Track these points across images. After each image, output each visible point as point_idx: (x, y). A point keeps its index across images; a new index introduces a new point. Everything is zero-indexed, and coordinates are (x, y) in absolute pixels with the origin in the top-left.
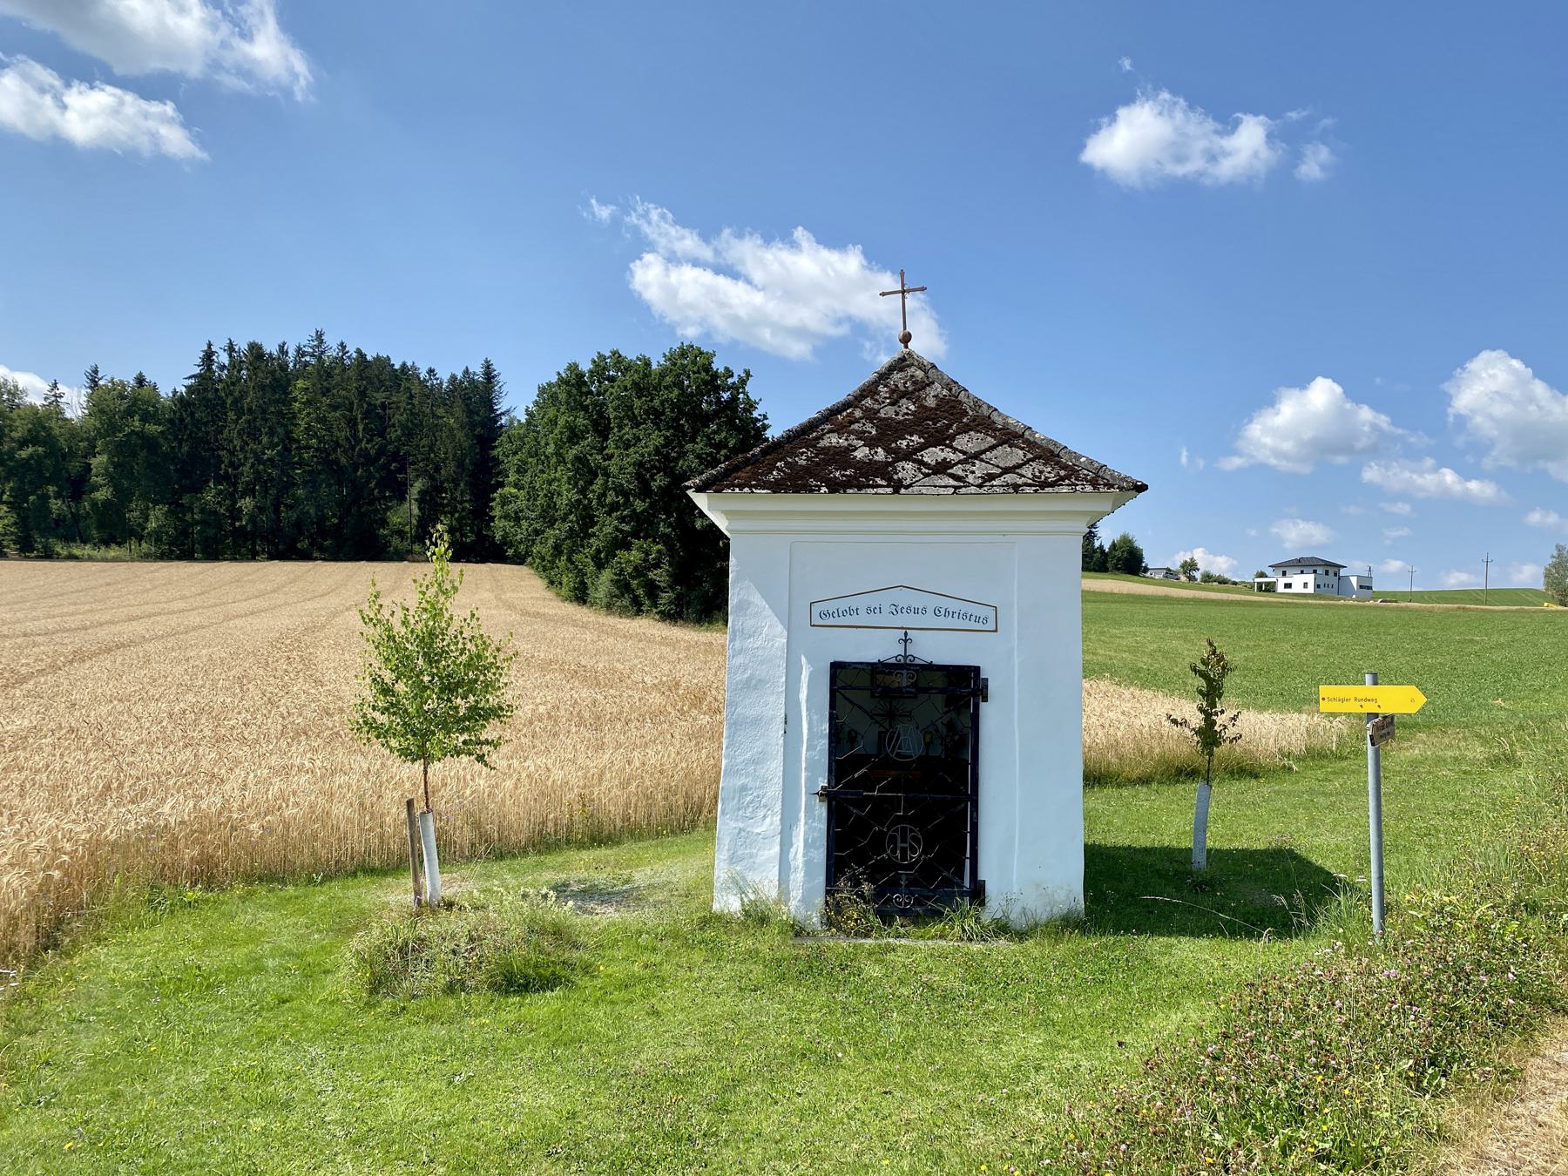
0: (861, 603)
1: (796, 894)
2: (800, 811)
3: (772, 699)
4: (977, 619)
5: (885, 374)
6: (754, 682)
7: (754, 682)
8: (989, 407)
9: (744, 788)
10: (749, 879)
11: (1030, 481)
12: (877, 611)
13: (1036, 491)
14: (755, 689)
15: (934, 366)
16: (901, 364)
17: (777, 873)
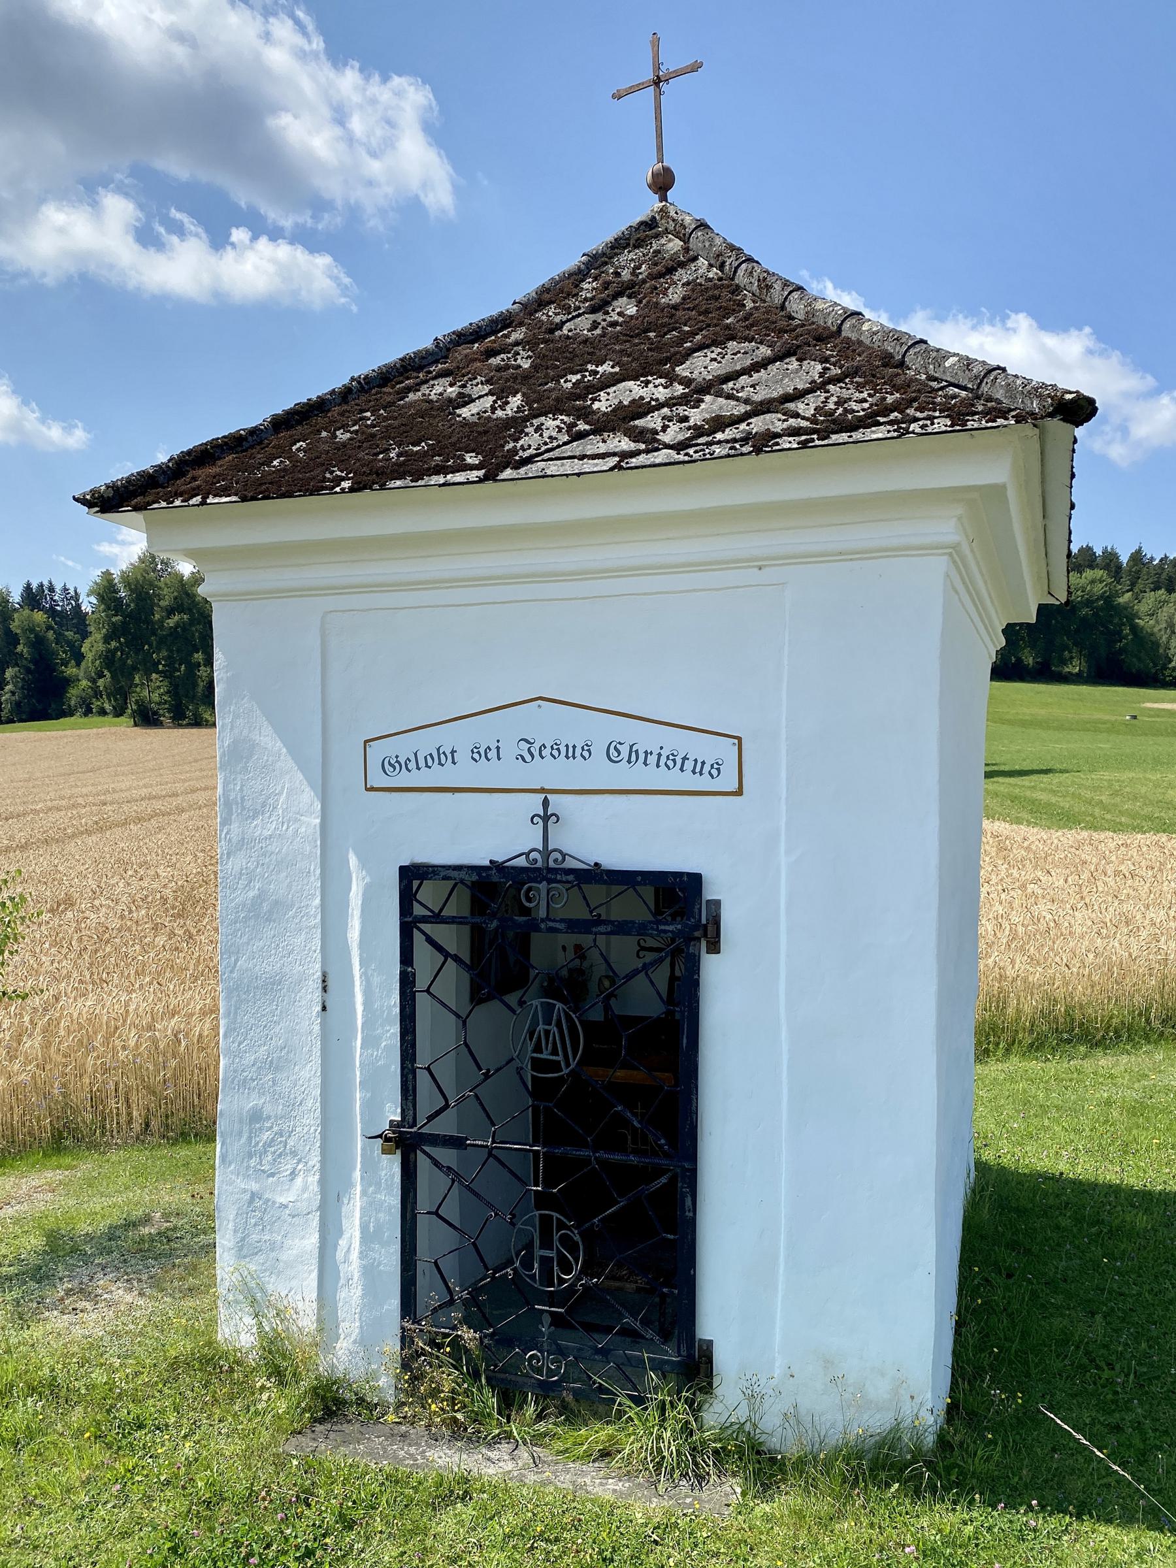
0: (459, 737)
1: (349, 1329)
2: (354, 1168)
3: (300, 940)
4: (698, 768)
5: (604, 254)
6: (265, 907)
7: (265, 907)
8: (786, 283)
9: (256, 1116)
10: (270, 1288)
11: (804, 424)
12: (492, 754)
13: (804, 445)
14: (269, 920)
15: (702, 225)
16: (648, 229)
17: (315, 1284)
